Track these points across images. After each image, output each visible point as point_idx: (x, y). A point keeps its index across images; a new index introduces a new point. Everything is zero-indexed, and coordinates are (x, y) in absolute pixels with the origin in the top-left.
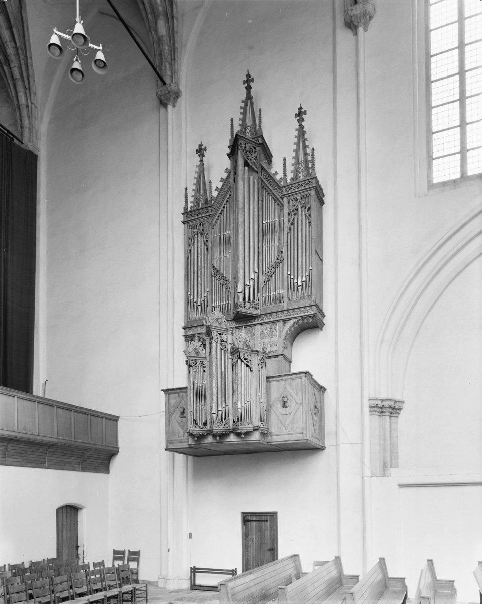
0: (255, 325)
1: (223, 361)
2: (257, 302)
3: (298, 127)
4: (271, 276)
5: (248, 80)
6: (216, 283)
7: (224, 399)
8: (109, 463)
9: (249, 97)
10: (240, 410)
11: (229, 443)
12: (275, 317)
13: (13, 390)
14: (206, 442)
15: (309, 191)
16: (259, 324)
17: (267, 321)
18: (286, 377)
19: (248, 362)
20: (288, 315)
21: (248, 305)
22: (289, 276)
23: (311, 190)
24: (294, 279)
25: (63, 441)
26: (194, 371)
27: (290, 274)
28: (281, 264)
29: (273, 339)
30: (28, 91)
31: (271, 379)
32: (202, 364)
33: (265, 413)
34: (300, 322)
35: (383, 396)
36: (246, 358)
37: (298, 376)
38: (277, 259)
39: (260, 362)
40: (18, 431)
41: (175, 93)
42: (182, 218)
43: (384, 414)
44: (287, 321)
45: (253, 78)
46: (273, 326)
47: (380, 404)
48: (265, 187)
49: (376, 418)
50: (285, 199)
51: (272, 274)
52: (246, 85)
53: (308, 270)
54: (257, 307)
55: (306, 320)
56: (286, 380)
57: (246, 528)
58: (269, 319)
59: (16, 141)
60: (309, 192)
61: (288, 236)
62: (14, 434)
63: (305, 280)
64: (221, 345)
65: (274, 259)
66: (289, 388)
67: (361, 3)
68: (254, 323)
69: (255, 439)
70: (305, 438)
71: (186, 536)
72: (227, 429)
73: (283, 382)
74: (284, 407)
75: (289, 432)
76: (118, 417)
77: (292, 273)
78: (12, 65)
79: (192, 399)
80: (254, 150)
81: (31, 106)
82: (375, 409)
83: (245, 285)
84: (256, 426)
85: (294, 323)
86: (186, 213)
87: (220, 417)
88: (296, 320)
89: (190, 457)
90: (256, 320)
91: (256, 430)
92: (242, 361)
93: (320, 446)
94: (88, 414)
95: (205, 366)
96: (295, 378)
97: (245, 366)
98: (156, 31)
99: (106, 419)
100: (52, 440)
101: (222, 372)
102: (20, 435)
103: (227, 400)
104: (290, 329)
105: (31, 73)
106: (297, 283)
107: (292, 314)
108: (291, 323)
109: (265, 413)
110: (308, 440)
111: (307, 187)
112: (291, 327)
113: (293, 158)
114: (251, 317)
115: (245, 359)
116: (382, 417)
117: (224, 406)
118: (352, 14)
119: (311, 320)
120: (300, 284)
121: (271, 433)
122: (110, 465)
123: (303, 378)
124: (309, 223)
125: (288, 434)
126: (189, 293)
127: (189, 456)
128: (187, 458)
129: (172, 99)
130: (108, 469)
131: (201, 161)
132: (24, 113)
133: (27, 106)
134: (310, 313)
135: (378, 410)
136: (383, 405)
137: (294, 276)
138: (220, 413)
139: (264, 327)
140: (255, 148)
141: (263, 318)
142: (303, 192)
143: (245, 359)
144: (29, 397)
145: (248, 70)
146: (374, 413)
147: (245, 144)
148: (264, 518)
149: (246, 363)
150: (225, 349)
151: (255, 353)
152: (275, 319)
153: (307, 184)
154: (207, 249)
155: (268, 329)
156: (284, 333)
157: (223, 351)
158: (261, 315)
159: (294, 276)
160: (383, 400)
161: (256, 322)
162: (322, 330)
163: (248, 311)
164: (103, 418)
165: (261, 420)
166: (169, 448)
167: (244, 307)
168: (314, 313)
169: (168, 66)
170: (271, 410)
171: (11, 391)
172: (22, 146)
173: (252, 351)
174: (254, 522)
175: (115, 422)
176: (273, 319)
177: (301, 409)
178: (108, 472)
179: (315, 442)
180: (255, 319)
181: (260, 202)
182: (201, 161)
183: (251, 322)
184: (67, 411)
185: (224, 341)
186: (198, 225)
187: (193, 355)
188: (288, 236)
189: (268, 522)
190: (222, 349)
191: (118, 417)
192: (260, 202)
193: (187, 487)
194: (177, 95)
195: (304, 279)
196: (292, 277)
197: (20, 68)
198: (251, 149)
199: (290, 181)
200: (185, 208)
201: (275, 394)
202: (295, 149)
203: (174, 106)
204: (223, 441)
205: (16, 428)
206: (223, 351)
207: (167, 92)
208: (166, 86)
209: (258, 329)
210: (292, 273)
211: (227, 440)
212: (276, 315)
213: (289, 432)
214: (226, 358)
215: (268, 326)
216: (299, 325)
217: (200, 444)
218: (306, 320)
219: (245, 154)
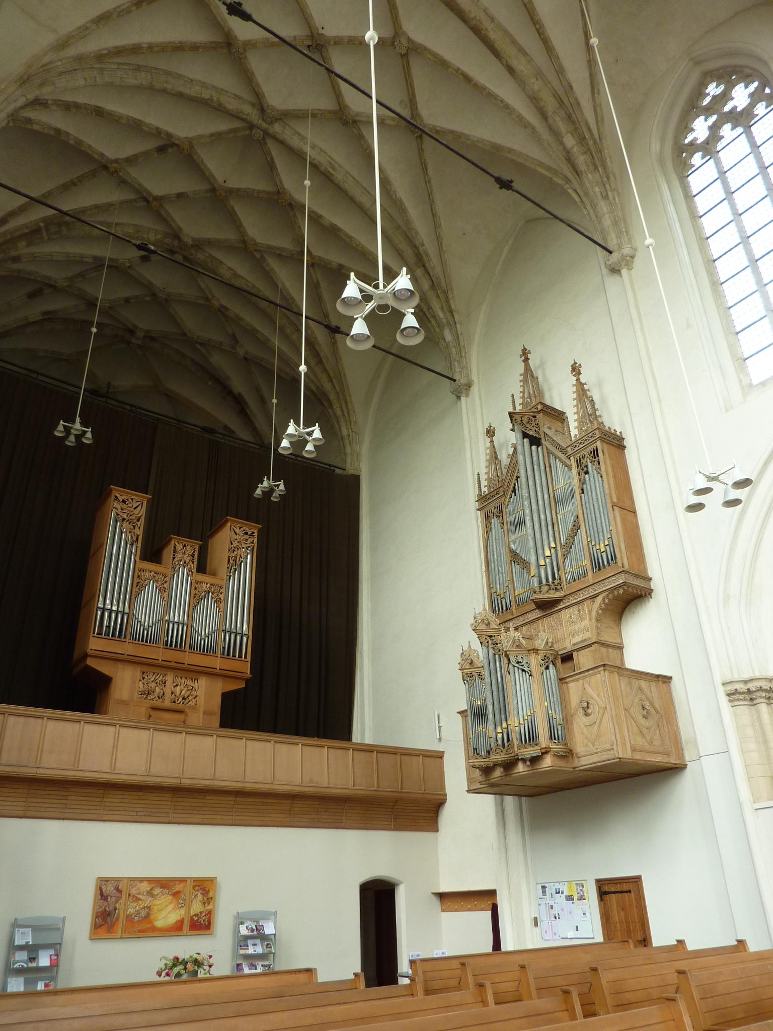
0: (560, 610)
1: (498, 669)
2: (559, 581)
3: (575, 383)
4: (571, 546)
5: (525, 353)
6: (517, 568)
7: (503, 717)
8: (437, 817)
9: (528, 369)
10: (517, 728)
11: (518, 774)
12: (581, 595)
13: (289, 736)
14: (495, 776)
15: (595, 443)
16: (566, 608)
17: (573, 602)
18: (583, 675)
19: (523, 666)
20: (595, 590)
21: (545, 588)
22: (590, 543)
23: (596, 442)
24: (595, 545)
25: (386, 794)
26: (470, 686)
27: (591, 541)
28: (579, 530)
29: (583, 624)
30: (348, 423)
31: (568, 680)
32: (479, 675)
33: (559, 728)
34: (610, 596)
35: (746, 676)
36: (520, 660)
37: (595, 670)
38: (574, 526)
39: (543, 662)
40: (302, 785)
41: (466, 385)
42: (477, 505)
43: (755, 702)
44: (595, 597)
45: (529, 351)
46: (581, 608)
47: (742, 687)
48: (585, 438)
49: (744, 711)
50: (572, 458)
51: (571, 544)
52: (523, 358)
53: (608, 530)
54: (559, 587)
55: (616, 593)
56: (584, 678)
57: (605, 904)
58: (575, 599)
59: (338, 471)
60: (595, 445)
61: (581, 497)
62: (297, 789)
63: (544, 563)
64: (494, 649)
65: (570, 526)
66: (590, 690)
67: (616, 251)
68: (560, 607)
69: (546, 766)
70: (617, 756)
71: (529, 923)
72: (511, 755)
73: (581, 682)
74: (586, 715)
75: (597, 749)
76: (443, 752)
77: (593, 539)
78: (335, 407)
79: (470, 722)
80: (533, 419)
81: (352, 435)
82: (736, 697)
83: (539, 566)
84: (544, 746)
85: (604, 599)
86: (482, 498)
87: (500, 742)
88: (605, 594)
89: (509, 801)
90: (562, 603)
91: (546, 753)
92: (514, 666)
93: (673, 763)
94: (397, 754)
95: (483, 677)
96: (594, 674)
97: (520, 671)
98: (444, 339)
99: (424, 756)
100: (346, 791)
101: (498, 683)
102: (307, 789)
103: (508, 717)
104: (600, 607)
105: (350, 408)
106: (600, 549)
107: (600, 588)
108: (599, 599)
109: (559, 728)
110: (620, 758)
111: (592, 440)
112: (600, 604)
113: (575, 413)
114: (556, 602)
115: (518, 662)
116: (753, 708)
117: (504, 725)
118: (610, 263)
119: (621, 591)
120: (603, 549)
121: (576, 754)
122: (439, 820)
123: (602, 672)
124: (601, 477)
125: (597, 753)
126: (491, 586)
127: (523, 798)
128: (520, 802)
129: (463, 391)
130: (437, 826)
131: (578, 380)
132: (347, 442)
133: (349, 436)
134: (619, 583)
135: (764, 695)
136: (749, 689)
137: (595, 542)
138: (500, 736)
139: (571, 610)
140: (535, 417)
141: (569, 599)
142: (591, 445)
143: (518, 662)
144: (316, 743)
145: (523, 345)
146: (736, 703)
147: (521, 418)
148: (625, 887)
149: (520, 667)
150: (499, 653)
151: (532, 651)
152: (582, 598)
153: (591, 436)
154: (504, 531)
155: (577, 612)
156: (594, 614)
157: (497, 656)
158: (564, 596)
159: (595, 542)
160: (746, 682)
161: (562, 605)
162: (651, 598)
163: (546, 596)
164: (419, 756)
165: (552, 737)
166: (471, 788)
167: (540, 592)
168: (622, 581)
169: (456, 364)
170: (573, 720)
171: (295, 739)
172: (345, 473)
173: (529, 650)
174: (613, 895)
175: (438, 760)
176: (580, 599)
177: (607, 715)
178: (436, 830)
179: (673, 760)
180: (560, 603)
181: (548, 469)
182: (492, 441)
183: (557, 607)
184: (367, 754)
185: (497, 644)
186: (493, 509)
187: (467, 667)
188: (581, 497)
189: (632, 892)
190: (495, 654)
191: (443, 752)
192: (548, 469)
193: (524, 845)
194: (469, 385)
195: (607, 543)
196: (593, 543)
197: (341, 407)
198: (530, 419)
199: (574, 439)
200: (480, 495)
201: (574, 699)
202: (575, 404)
203: (467, 396)
204: (509, 773)
205: (351, 782)
206: (497, 656)
207: (458, 387)
208: (457, 382)
209: (565, 614)
210: (593, 539)
211: (516, 771)
212: (582, 593)
213: (597, 749)
214: (502, 664)
215: (576, 608)
216: (609, 599)
217: (489, 780)
218: (616, 593)
219: (523, 426)
